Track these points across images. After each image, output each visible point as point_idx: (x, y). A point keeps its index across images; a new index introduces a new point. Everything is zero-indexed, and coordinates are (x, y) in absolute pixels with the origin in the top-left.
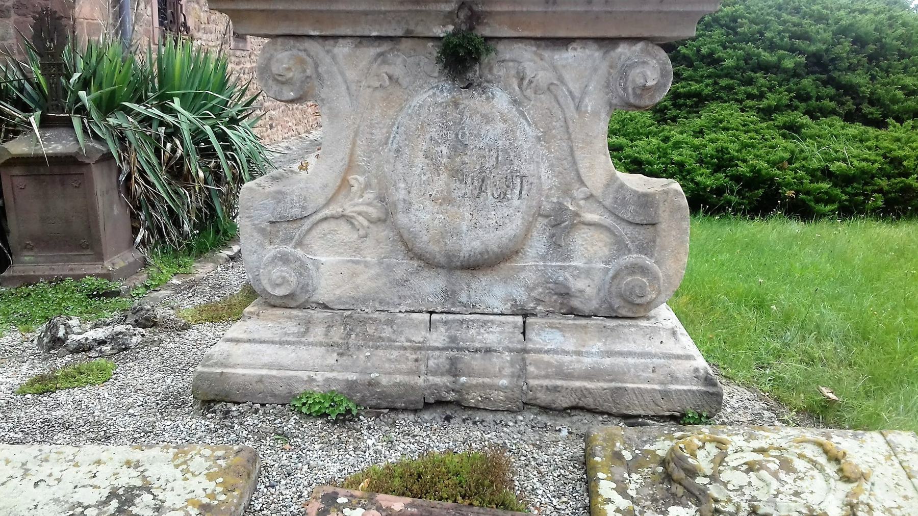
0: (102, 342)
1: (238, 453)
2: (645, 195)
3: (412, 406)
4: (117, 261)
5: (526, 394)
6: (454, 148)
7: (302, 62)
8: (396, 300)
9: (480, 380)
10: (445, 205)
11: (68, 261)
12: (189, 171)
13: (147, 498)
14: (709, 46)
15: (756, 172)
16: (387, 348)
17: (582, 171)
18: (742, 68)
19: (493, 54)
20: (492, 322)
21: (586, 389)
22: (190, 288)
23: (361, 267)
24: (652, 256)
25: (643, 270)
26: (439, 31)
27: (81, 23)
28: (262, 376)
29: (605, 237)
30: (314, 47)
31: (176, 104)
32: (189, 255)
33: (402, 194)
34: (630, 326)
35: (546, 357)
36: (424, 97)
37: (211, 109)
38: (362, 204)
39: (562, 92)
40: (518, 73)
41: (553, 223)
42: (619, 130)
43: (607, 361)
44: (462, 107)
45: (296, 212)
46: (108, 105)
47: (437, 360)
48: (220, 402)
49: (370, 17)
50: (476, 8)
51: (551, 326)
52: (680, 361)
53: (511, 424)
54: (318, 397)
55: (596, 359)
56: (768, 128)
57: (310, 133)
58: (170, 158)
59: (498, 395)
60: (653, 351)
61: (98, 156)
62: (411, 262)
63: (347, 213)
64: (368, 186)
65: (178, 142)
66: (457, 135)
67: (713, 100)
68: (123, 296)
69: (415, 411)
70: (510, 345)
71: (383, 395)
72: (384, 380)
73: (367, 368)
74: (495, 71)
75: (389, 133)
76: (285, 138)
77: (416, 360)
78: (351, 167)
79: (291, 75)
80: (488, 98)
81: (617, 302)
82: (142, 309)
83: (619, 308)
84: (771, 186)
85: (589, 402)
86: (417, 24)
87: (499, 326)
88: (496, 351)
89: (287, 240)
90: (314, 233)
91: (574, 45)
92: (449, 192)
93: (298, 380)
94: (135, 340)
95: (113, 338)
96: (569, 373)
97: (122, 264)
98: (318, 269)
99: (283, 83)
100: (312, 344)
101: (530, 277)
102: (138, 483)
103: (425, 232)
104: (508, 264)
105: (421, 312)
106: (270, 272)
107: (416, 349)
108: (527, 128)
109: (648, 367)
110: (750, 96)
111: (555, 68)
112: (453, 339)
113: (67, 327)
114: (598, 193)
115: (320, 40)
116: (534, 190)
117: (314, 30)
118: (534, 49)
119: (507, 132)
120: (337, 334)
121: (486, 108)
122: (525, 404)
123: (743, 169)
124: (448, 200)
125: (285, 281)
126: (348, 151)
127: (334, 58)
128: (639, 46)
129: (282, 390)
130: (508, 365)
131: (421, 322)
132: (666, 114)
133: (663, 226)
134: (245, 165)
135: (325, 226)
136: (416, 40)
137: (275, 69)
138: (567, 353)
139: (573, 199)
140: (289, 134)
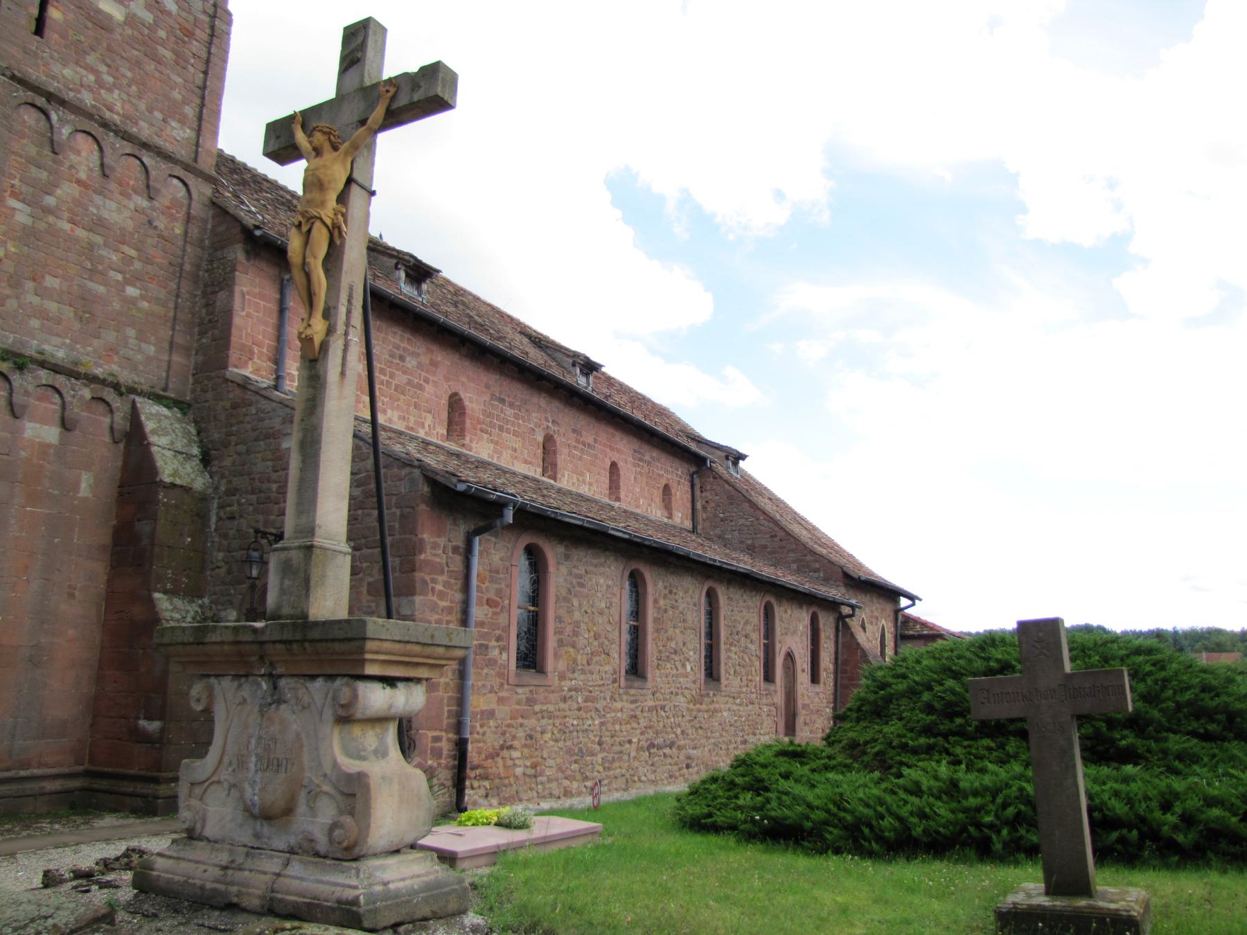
30: (213, 680)
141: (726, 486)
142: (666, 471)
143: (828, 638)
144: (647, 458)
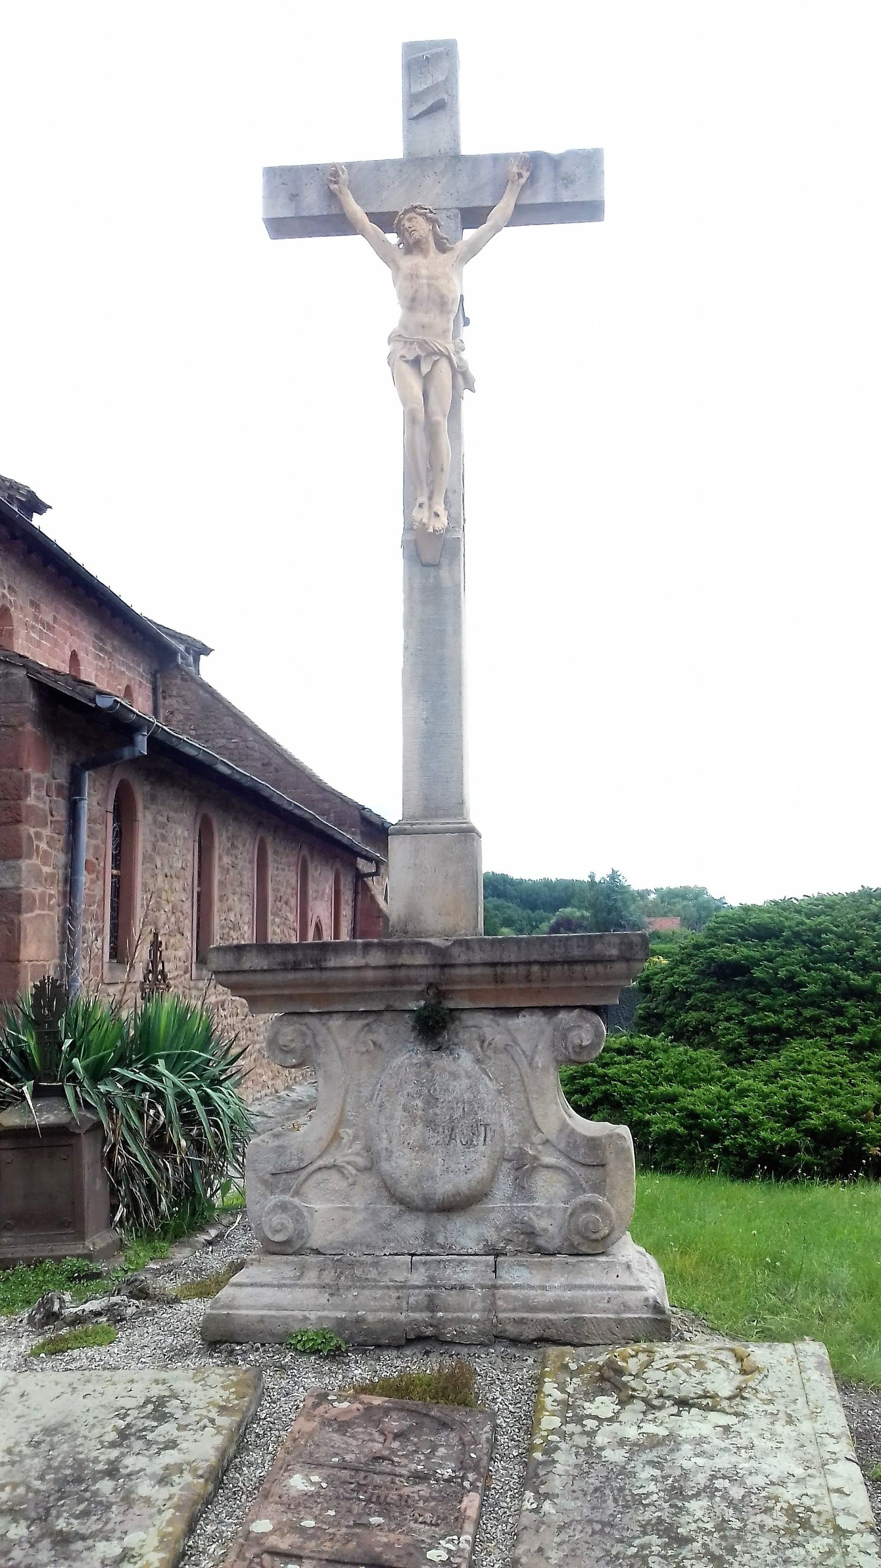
0: (98, 1314)
1: (246, 1371)
2: (593, 1139)
3: (395, 1343)
4: (97, 1241)
5: (496, 1326)
6: (427, 1103)
7: (303, 1034)
8: (381, 1244)
9: (455, 1315)
10: (420, 1153)
11: (48, 1241)
12: (171, 1140)
13: (176, 1402)
14: (788, 968)
15: (832, 1125)
16: (373, 1287)
17: (538, 1119)
18: (831, 995)
19: (457, 1023)
20: (466, 1261)
21: (550, 1320)
22: (170, 1272)
23: (350, 1214)
24: (604, 1195)
25: (595, 1207)
26: (413, 1006)
27: (26, 966)
28: (262, 1316)
29: (562, 1178)
30: (314, 1022)
31: (161, 1066)
32: (164, 1239)
33: (385, 1143)
34: (591, 1262)
35: (514, 1292)
36: (402, 1059)
37: (192, 1070)
38: (352, 1154)
39: (517, 1052)
40: (479, 1037)
41: (516, 1166)
42: (675, 1076)
43: (568, 1294)
44: (433, 1066)
45: (294, 1163)
46: (97, 1073)
47: (417, 1297)
48: (225, 1342)
49: (358, 997)
50: (440, 988)
51: (520, 1264)
52: (633, 1292)
53: (483, 1356)
54: (311, 1335)
55: (558, 1292)
56: (860, 1069)
57: (292, 1090)
58: (152, 1127)
59: (471, 1328)
60: (609, 1284)
61: (89, 1125)
62: (394, 1207)
63: (338, 1162)
64: (356, 1138)
65: (160, 1109)
66: (429, 1091)
67: (798, 1035)
68: (105, 1278)
69: (398, 1347)
70: (482, 1282)
71: (369, 1332)
72: (370, 1317)
73: (355, 1306)
74: (461, 1035)
75: (374, 1090)
76: (257, 1099)
77: (398, 1298)
78: (341, 1121)
79: (294, 1045)
80: (454, 1059)
81: (576, 1240)
82: (136, 1280)
83: (578, 1244)
84: (853, 1142)
85: (552, 1333)
86: (395, 1001)
87: (473, 1265)
88: (469, 1288)
89: (284, 1191)
90: (311, 1182)
91: (524, 1013)
92: (424, 1141)
93: (296, 1320)
94: (130, 1311)
95: (109, 1310)
96: (534, 1306)
97: (103, 1245)
98: (312, 1216)
99: (287, 1052)
100: (307, 1286)
101: (499, 1218)
102: (167, 1393)
103: (404, 1177)
104: (479, 1206)
105: (403, 1254)
106: (270, 1220)
107: (398, 1288)
108: (489, 1083)
109: (604, 1299)
110: (840, 1030)
111: (509, 1031)
112: (432, 1278)
113: (62, 1301)
114: (552, 1137)
115: (319, 1016)
116: (497, 1136)
117: (313, 1008)
118: (491, 1016)
119: (471, 1087)
120: (328, 1277)
121: (453, 1067)
122: (496, 1337)
123: (814, 1121)
124: (424, 1148)
125: (283, 1228)
126: (339, 1108)
127: (328, 1029)
128: (576, 1011)
129: (279, 1330)
130: (480, 1300)
131: (403, 1263)
132: (740, 1054)
133: (611, 1166)
134: (228, 1131)
135: (319, 1176)
136: (394, 1014)
137: (282, 1041)
138: (532, 1287)
139: (532, 1144)
140: (263, 1092)
141: (201, 692)
142: (129, 668)
143: (347, 901)
144: (108, 648)
